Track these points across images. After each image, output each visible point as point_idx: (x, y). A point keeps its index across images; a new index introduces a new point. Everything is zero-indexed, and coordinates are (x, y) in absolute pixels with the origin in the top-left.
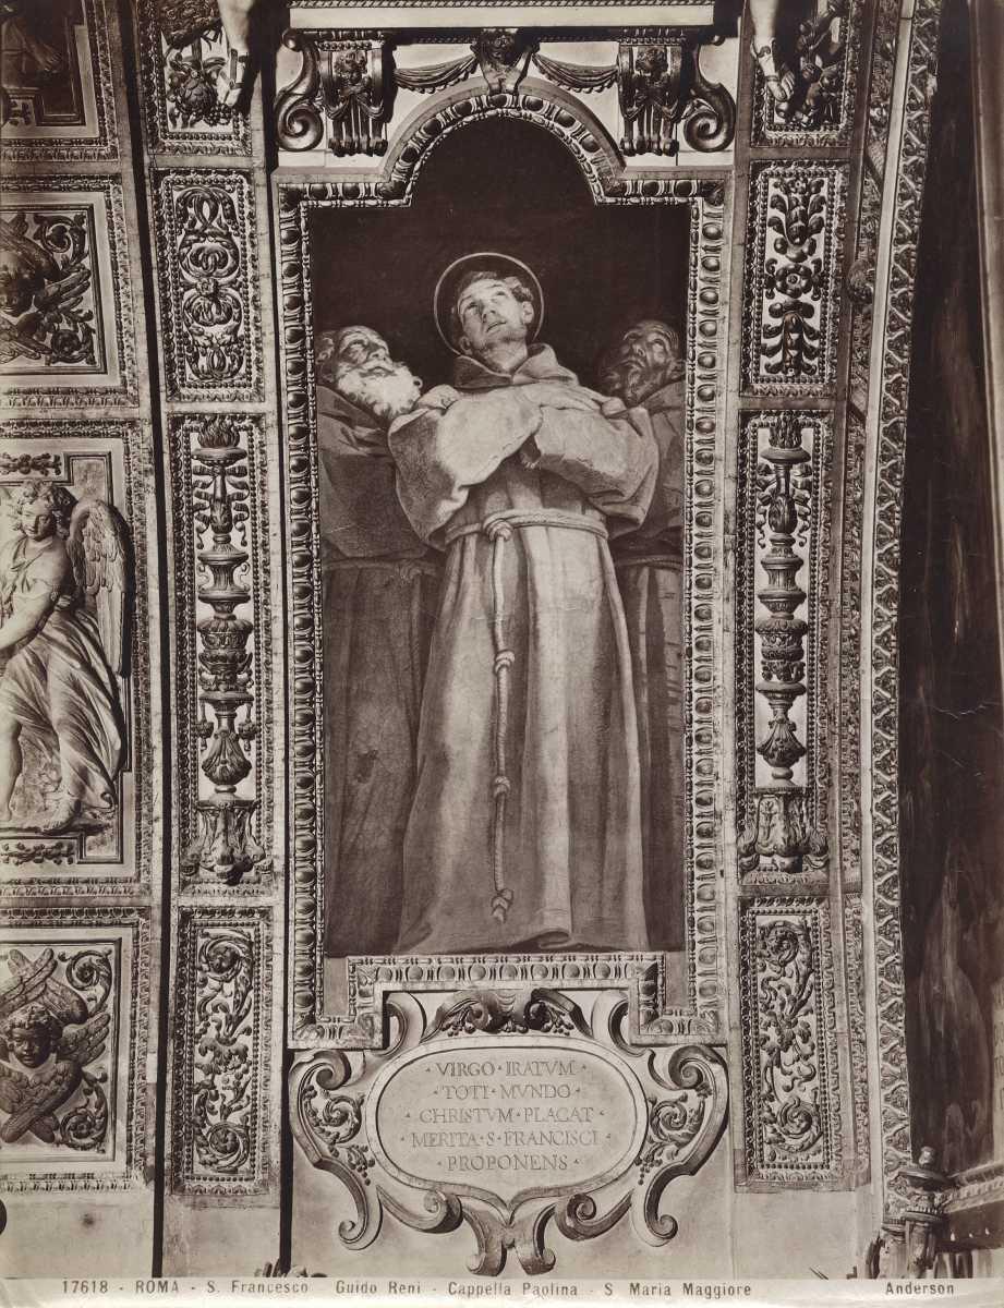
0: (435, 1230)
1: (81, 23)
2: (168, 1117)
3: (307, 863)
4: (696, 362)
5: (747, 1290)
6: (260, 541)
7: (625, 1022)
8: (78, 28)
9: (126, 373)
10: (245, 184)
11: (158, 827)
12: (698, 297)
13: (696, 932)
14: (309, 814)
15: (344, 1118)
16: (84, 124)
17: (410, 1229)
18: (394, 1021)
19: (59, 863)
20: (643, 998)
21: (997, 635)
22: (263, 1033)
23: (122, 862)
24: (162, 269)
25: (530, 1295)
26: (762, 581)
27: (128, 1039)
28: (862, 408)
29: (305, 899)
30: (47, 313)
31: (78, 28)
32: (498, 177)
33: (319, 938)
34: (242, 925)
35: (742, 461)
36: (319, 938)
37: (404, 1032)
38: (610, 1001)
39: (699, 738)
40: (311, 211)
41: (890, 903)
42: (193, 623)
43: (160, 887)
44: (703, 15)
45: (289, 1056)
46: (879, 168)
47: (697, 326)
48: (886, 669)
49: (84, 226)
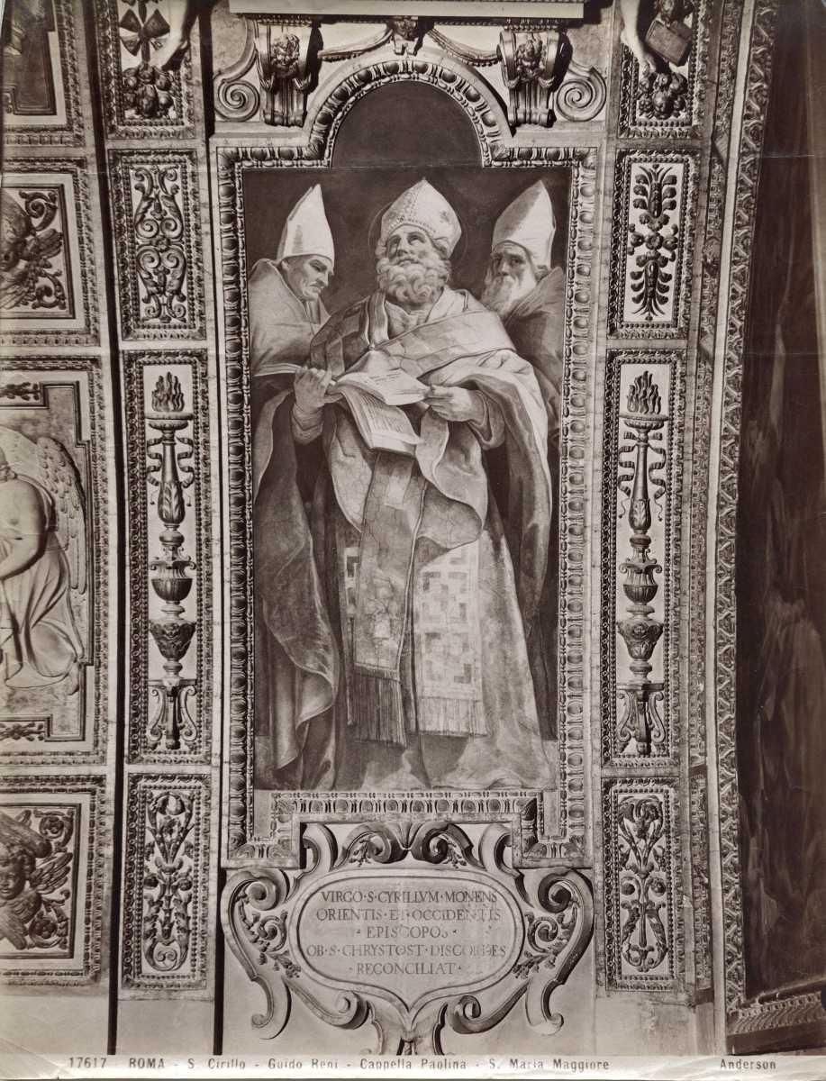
0: (346, 1026)
1: (53, 30)
2: (122, 375)
3: (240, 697)
4: (566, 685)
5: (606, 1065)
6: (203, 538)
7: (508, 851)
8: (50, 34)
9: (90, 925)
10: (188, 163)
11: (113, 729)
12: (568, 480)
13: (566, 689)
14: (243, 656)
15: (274, 933)
16: (55, 113)
17: (326, 990)
18: (310, 853)
19: (31, 740)
20: (525, 823)
21: (821, 439)
22: (205, 568)
23: (84, 739)
24: (124, 286)
25: (427, 1068)
26: (622, 578)
27: (86, 860)
28: (710, 350)
29: (237, 777)
30: (27, 258)
31: (50, 34)
32: (398, 132)
33: (250, 707)
34: (180, 788)
35: (606, 730)
36: (250, 707)
37: (317, 859)
38: (495, 834)
39: (570, 735)
40: (246, 174)
41: (728, 566)
42: (142, 413)
43: (112, 424)
44: (577, 12)
45: (222, 873)
46: (724, 155)
47: (575, 269)
48: (727, 717)
49: (57, 204)
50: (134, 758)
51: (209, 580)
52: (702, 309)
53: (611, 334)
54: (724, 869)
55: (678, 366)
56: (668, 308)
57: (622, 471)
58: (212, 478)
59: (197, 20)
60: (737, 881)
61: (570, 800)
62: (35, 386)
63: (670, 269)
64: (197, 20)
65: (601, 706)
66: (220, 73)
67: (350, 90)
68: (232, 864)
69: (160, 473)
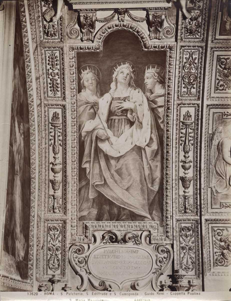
32: (122, 43)
50: (197, 221)
51: (179, 86)
52: (38, 61)
53: (62, 48)
54: (34, 125)
55: (46, 96)
56: (48, 55)
57: (61, 131)
58: (175, 139)
59: (180, 9)
60: (32, 189)
61: (75, 128)
62: (223, 207)
63: (48, 67)
64: (180, 9)
65: (66, 110)
66: (173, 36)
67: (134, 29)
68: (174, 43)
69: (189, 139)
